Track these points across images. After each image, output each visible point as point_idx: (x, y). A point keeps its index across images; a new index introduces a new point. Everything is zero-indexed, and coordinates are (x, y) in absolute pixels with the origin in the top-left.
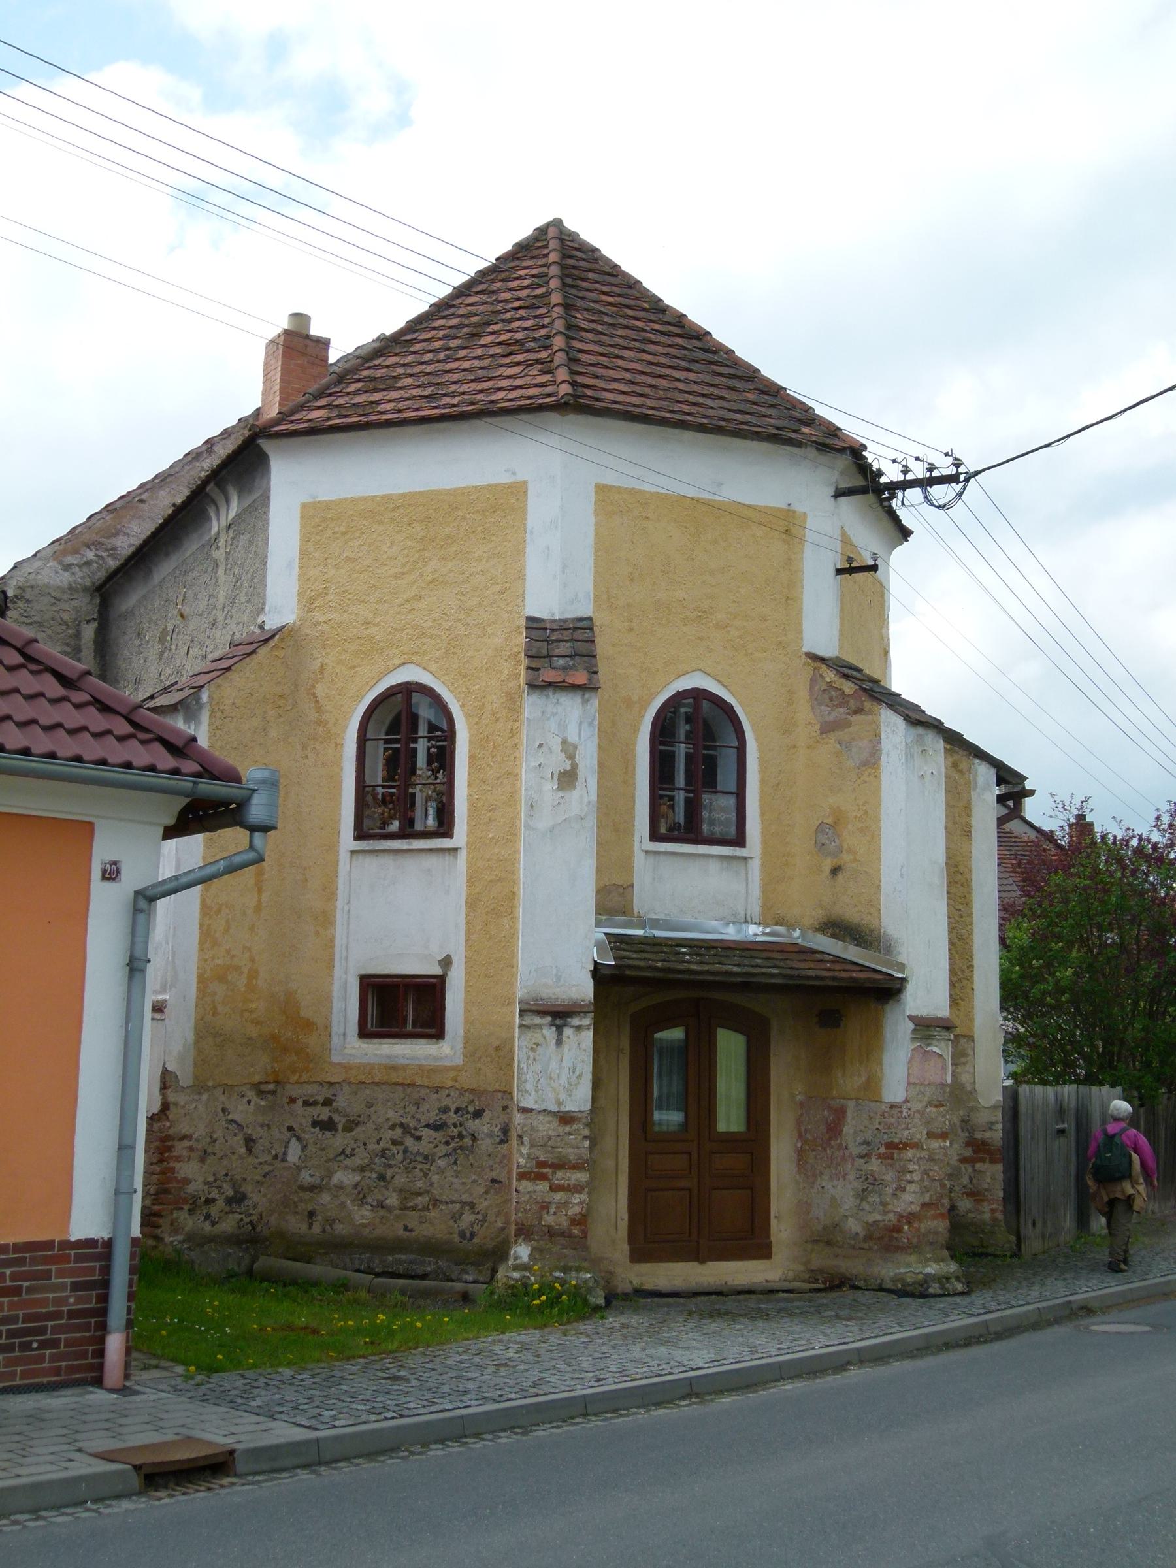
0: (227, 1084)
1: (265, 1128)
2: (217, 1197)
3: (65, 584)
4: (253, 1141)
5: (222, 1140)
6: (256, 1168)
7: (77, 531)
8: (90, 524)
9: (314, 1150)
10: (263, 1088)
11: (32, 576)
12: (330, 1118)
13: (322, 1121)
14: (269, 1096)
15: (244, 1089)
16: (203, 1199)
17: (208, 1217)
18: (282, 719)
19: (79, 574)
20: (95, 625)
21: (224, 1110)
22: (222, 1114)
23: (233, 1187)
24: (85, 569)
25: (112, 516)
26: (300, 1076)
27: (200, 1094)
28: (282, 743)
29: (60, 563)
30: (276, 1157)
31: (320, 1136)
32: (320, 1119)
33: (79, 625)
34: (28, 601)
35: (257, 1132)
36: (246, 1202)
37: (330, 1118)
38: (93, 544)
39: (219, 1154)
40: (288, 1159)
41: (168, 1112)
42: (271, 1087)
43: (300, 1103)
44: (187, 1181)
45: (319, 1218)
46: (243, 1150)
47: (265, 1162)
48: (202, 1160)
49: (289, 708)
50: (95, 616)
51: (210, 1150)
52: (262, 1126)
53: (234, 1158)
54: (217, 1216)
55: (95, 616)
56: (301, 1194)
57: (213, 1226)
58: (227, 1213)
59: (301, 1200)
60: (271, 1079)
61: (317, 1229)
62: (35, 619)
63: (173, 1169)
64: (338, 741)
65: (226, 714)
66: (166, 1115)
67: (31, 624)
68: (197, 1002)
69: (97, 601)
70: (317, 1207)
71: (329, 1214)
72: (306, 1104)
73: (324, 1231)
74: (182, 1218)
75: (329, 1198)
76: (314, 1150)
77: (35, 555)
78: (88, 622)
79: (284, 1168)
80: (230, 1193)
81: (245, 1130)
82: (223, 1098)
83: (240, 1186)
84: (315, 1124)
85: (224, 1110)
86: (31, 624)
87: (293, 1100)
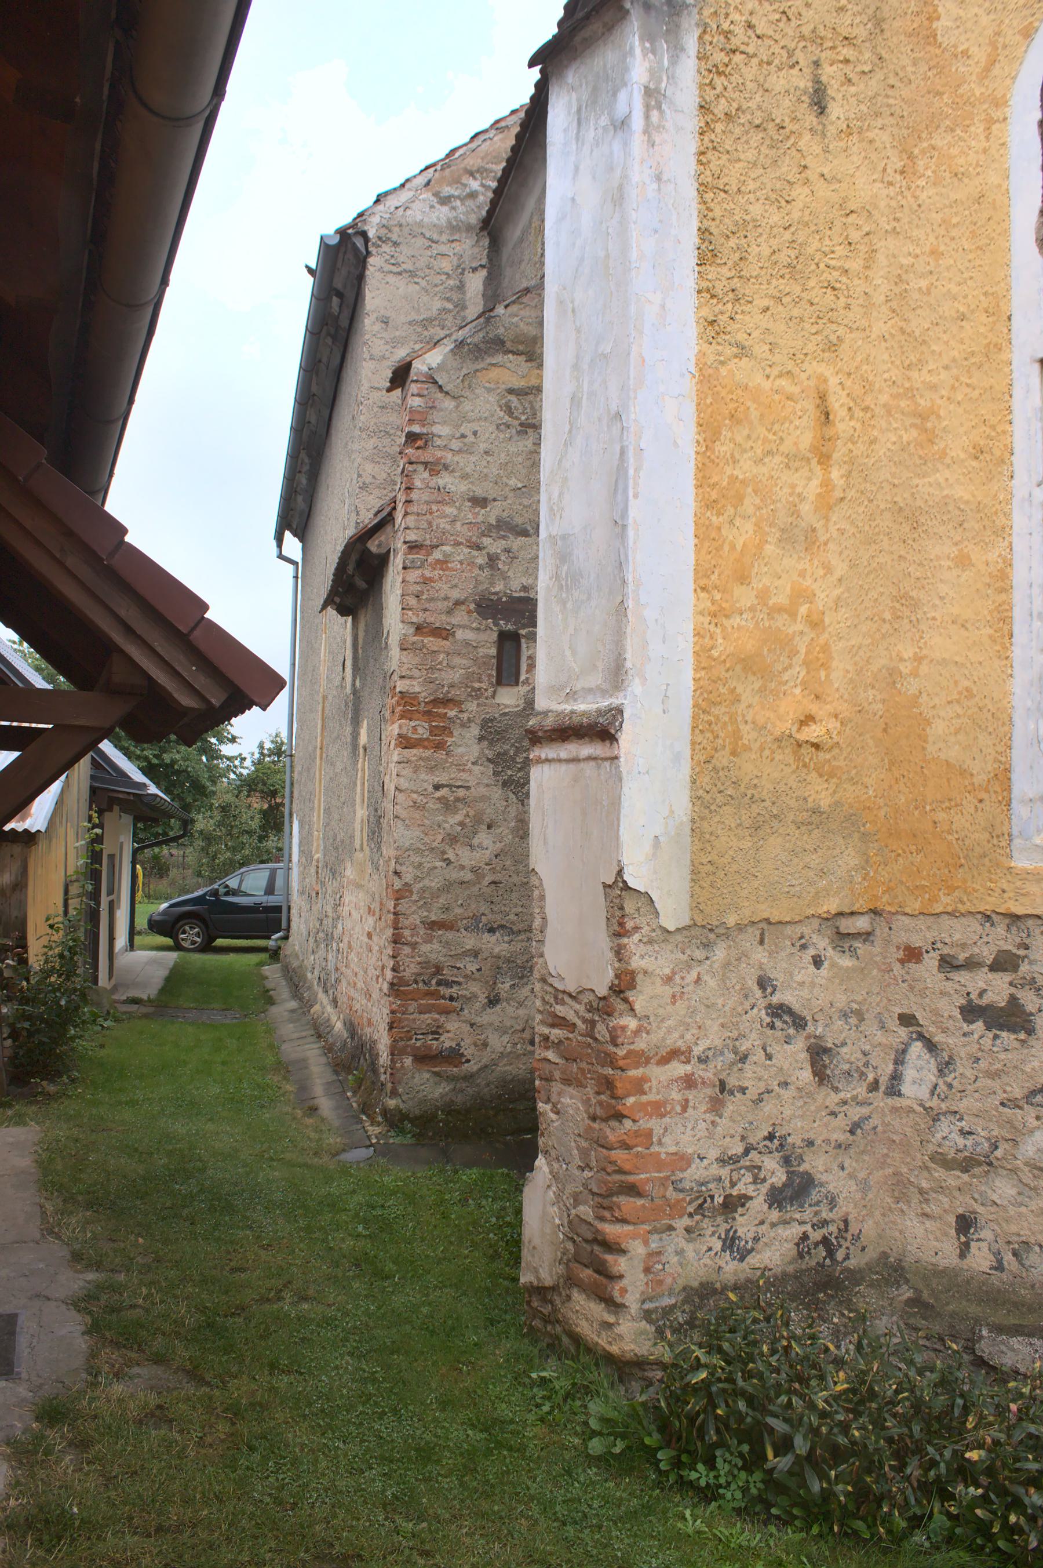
0: (767, 921)
1: (853, 1021)
2: (750, 1191)
3: (443, 222)
4: (826, 1051)
5: (759, 1055)
6: (833, 1114)
7: (457, 155)
8: (473, 145)
9: (969, 1073)
10: (847, 925)
11: (401, 211)
12: (1013, 999)
13: (989, 1007)
14: (857, 944)
15: (806, 930)
16: (719, 1200)
17: (730, 1242)
18: (853, 90)
19: (461, 209)
20: (484, 273)
21: (763, 983)
22: (758, 993)
23: (787, 1161)
24: (470, 203)
25: (501, 136)
26: (934, 899)
27: (707, 945)
28: (855, 138)
29: (436, 195)
30: (874, 1086)
31: (987, 1041)
32: (984, 1001)
33: (462, 274)
34: (396, 244)
35: (832, 1032)
36: (814, 1195)
37: (1013, 999)
38: (478, 171)
39: (752, 1093)
40: (906, 1088)
41: (631, 995)
42: (862, 923)
43: (931, 961)
44: (682, 1160)
45: (986, 1234)
46: (806, 1075)
47: (854, 1098)
48: (716, 1106)
49: (867, 69)
50: (484, 262)
51: (732, 1082)
52: (845, 1015)
53: (787, 1094)
54: (751, 1235)
55: (484, 262)
56: (939, 1173)
57: (742, 1259)
58: (773, 1225)
59: (941, 1189)
60: (860, 905)
61: (980, 1259)
62: (404, 266)
63: (649, 1134)
64: (997, 114)
65: (735, 42)
66: (626, 1000)
67: (400, 273)
68: (695, 717)
69: (486, 242)
70: (980, 1209)
71: (1013, 1228)
72: (947, 964)
73: (999, 1267)
74: (670, 1249)
75: (1013, 1192)
76: (969, 1073)
77: (403, 185)
78: (474, 270)
79: (895, 1110)
80: (779, 1177)
81: (810, 1028)
82: (760, 955)
83: (801, 1159)
84: (971, 1011)
85: (763, 983)
86: (400, 273)
87: (912, 955)
